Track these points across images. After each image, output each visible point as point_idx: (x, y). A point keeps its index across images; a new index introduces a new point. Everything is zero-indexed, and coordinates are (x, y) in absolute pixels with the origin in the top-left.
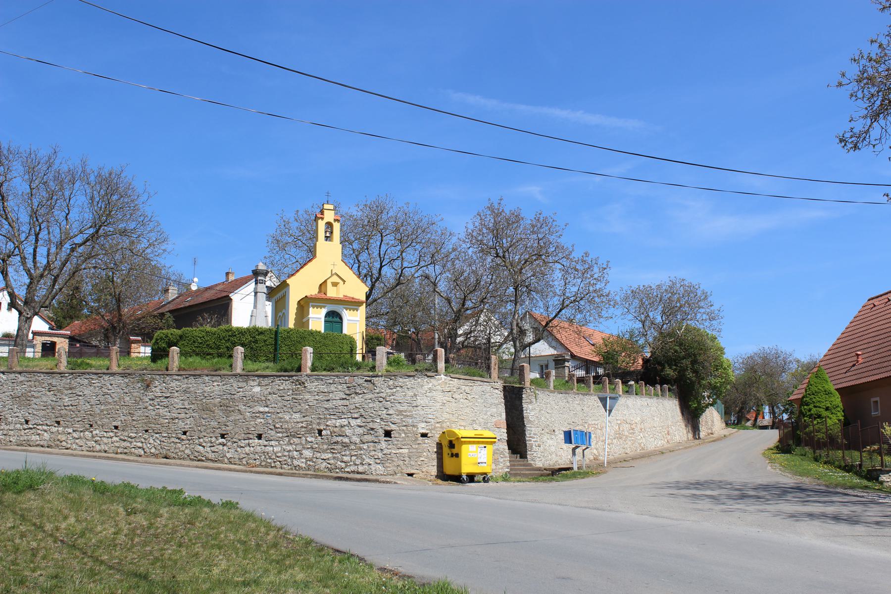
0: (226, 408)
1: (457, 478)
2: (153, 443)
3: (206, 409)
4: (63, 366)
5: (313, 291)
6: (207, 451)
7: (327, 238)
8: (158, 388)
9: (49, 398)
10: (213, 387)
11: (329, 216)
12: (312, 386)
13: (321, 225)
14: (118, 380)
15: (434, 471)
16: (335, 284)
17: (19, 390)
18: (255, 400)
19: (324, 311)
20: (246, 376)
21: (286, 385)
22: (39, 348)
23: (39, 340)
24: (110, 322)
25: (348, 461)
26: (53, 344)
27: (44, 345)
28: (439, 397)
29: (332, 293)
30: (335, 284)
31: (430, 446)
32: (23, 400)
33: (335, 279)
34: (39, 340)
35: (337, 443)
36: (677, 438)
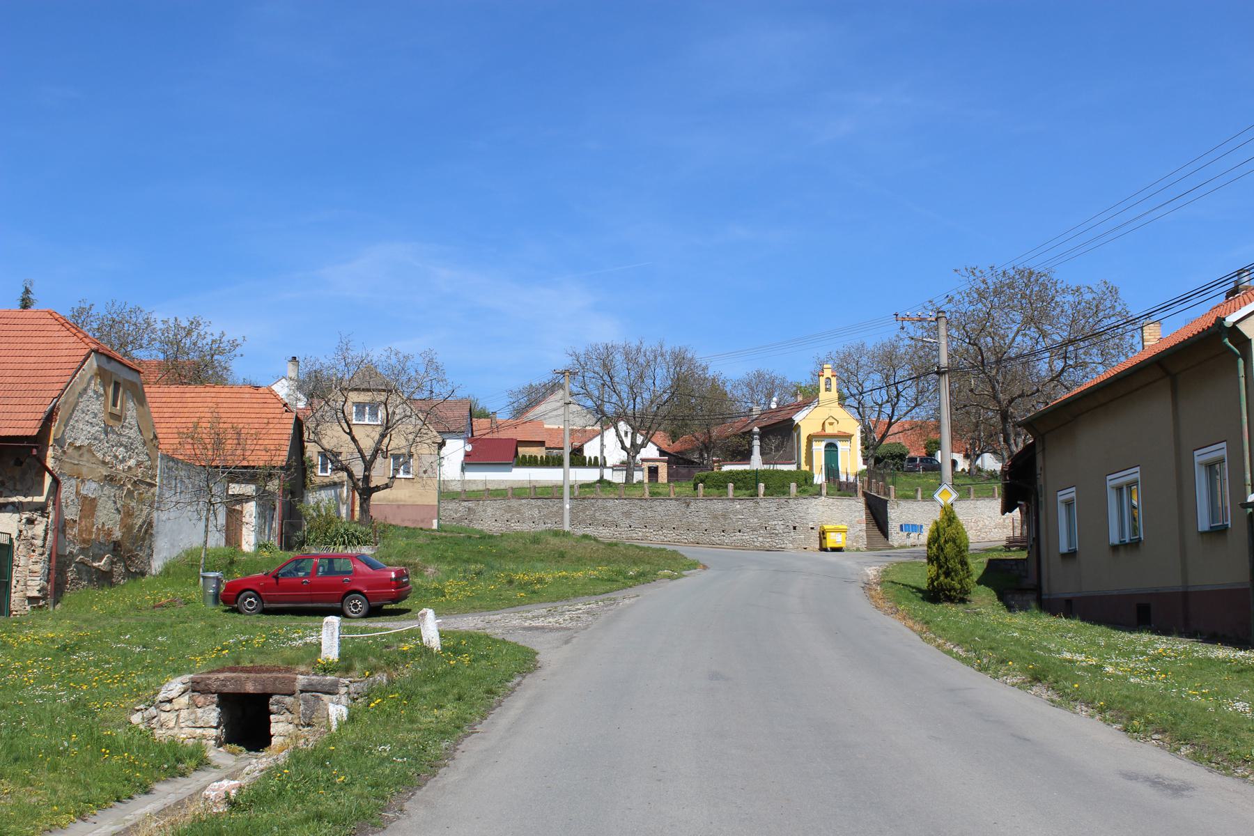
0: (724, 516)
1: (826, 550)
2: (691, 536)
3: (715, 517)
4: (647, 495)
5: (818, 429)
6: (716, 539)
7: (827, 390)
8: (693, 506)
9: (641, 513)
10: (718, 506)
11: (828, 373)
12: (762, 504)
13: (822, 380)
14: (674, 502)
15: (818, 546)
16: (831, 424)
17: (626, 509)
18: (736, 512)
19: (824, 444)
20: (733, 500)
21: (751, 504)
22: (646, 470)
23: (646, 465)
24: (703, 443)
25: (777, 542)
26: (656, 468)
27: (649, 468)
28: (821, 508)
29: (829, 430)
30: (831, 424)
31: (815, 534)
32: (627, 514)
33: (831, 420)
34: (646, 465)
35: (773, 534)
36: (254, 509)
